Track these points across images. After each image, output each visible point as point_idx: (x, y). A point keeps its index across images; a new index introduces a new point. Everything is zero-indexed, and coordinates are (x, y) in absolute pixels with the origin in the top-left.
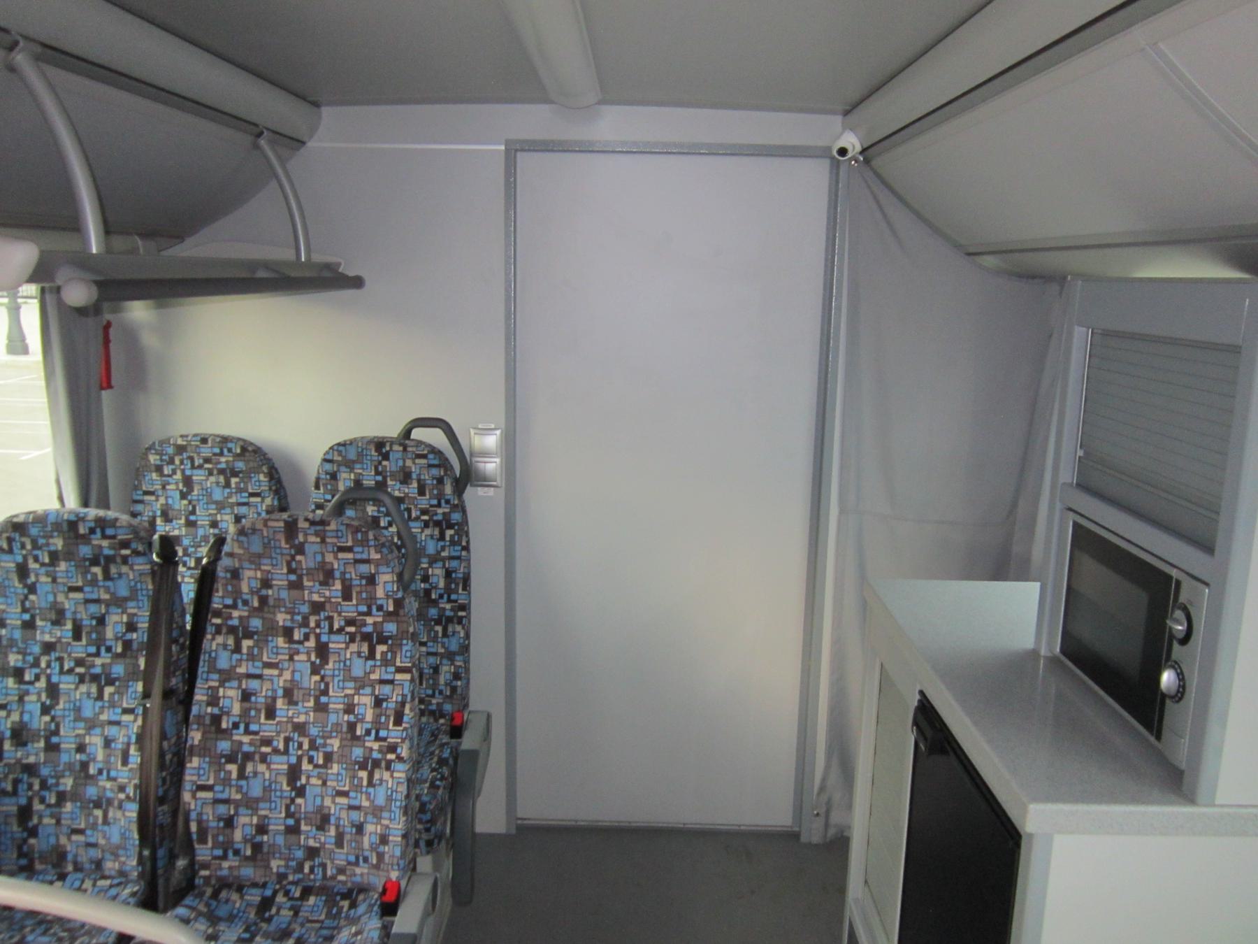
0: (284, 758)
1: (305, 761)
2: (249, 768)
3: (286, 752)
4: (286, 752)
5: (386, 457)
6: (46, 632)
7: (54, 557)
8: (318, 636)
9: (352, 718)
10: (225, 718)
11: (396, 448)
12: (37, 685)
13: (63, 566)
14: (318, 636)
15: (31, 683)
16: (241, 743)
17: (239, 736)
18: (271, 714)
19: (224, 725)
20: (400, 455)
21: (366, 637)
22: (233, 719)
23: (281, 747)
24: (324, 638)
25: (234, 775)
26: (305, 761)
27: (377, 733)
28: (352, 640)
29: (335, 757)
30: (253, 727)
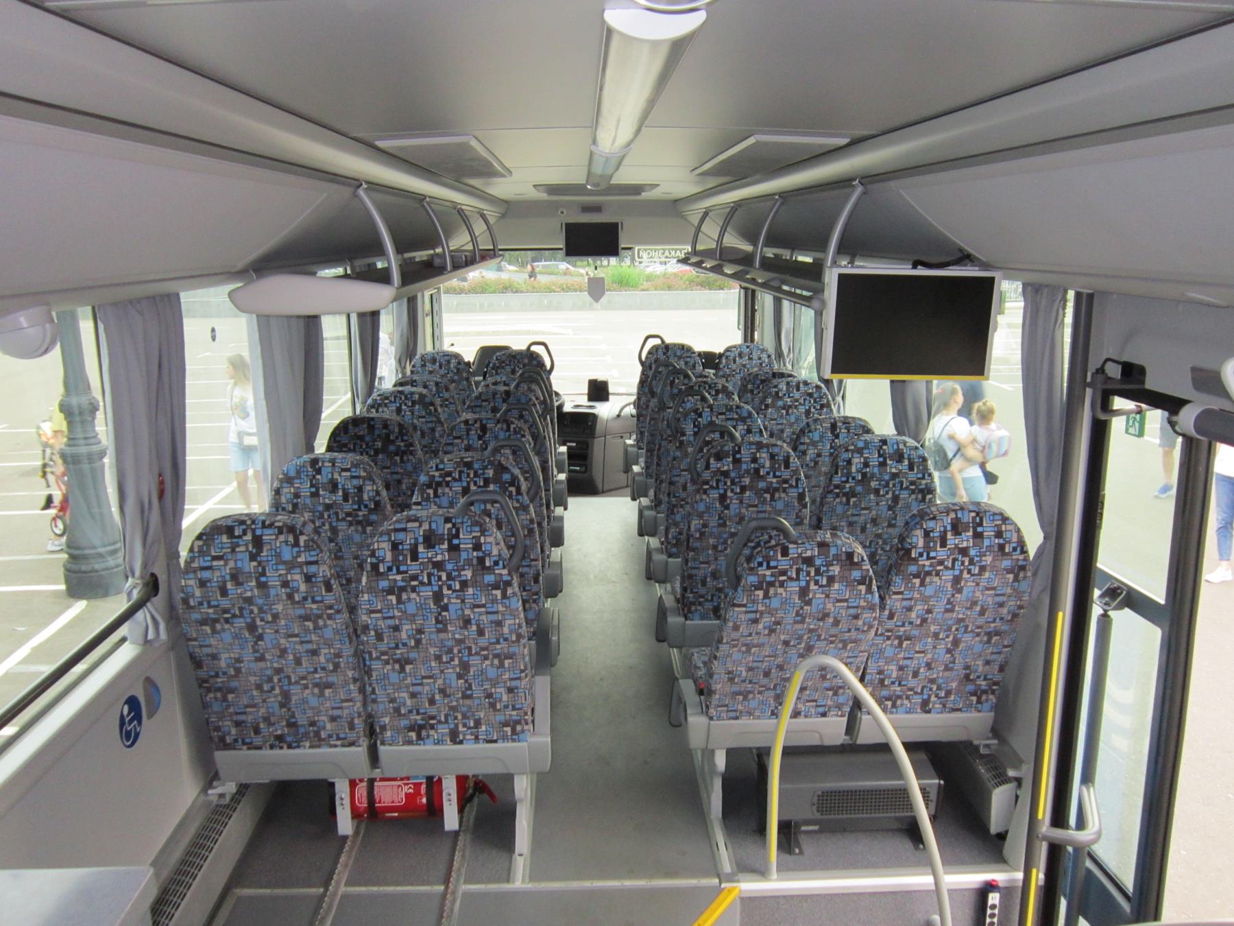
0: (429, 588)
1: (812, 584)
2: (404, 596)
3: (430, 583)
4: (430, 583)
5: (319, 471)
6: (326, 497)
7: (377, 452)
8: (254, 531)
9: (1001, 541)
10: (381, 566)
11: (327, 464)
12: (245, 538)
13: (380, 456)
14: (254, 531)
15: (240, 537)
16: (395, 580)
17: (924, 561)
18: (415, 557)
19: (488, 564)
20: (330, 470)
21: (845, 494)
22: (387, 565)
23: (426, 580)
24: (258, 532)
25: (394, 602)
26: (812, 584)
27: (398, 569)
28: (280, 532)
29: (837, 579)
30: (403, 568)
